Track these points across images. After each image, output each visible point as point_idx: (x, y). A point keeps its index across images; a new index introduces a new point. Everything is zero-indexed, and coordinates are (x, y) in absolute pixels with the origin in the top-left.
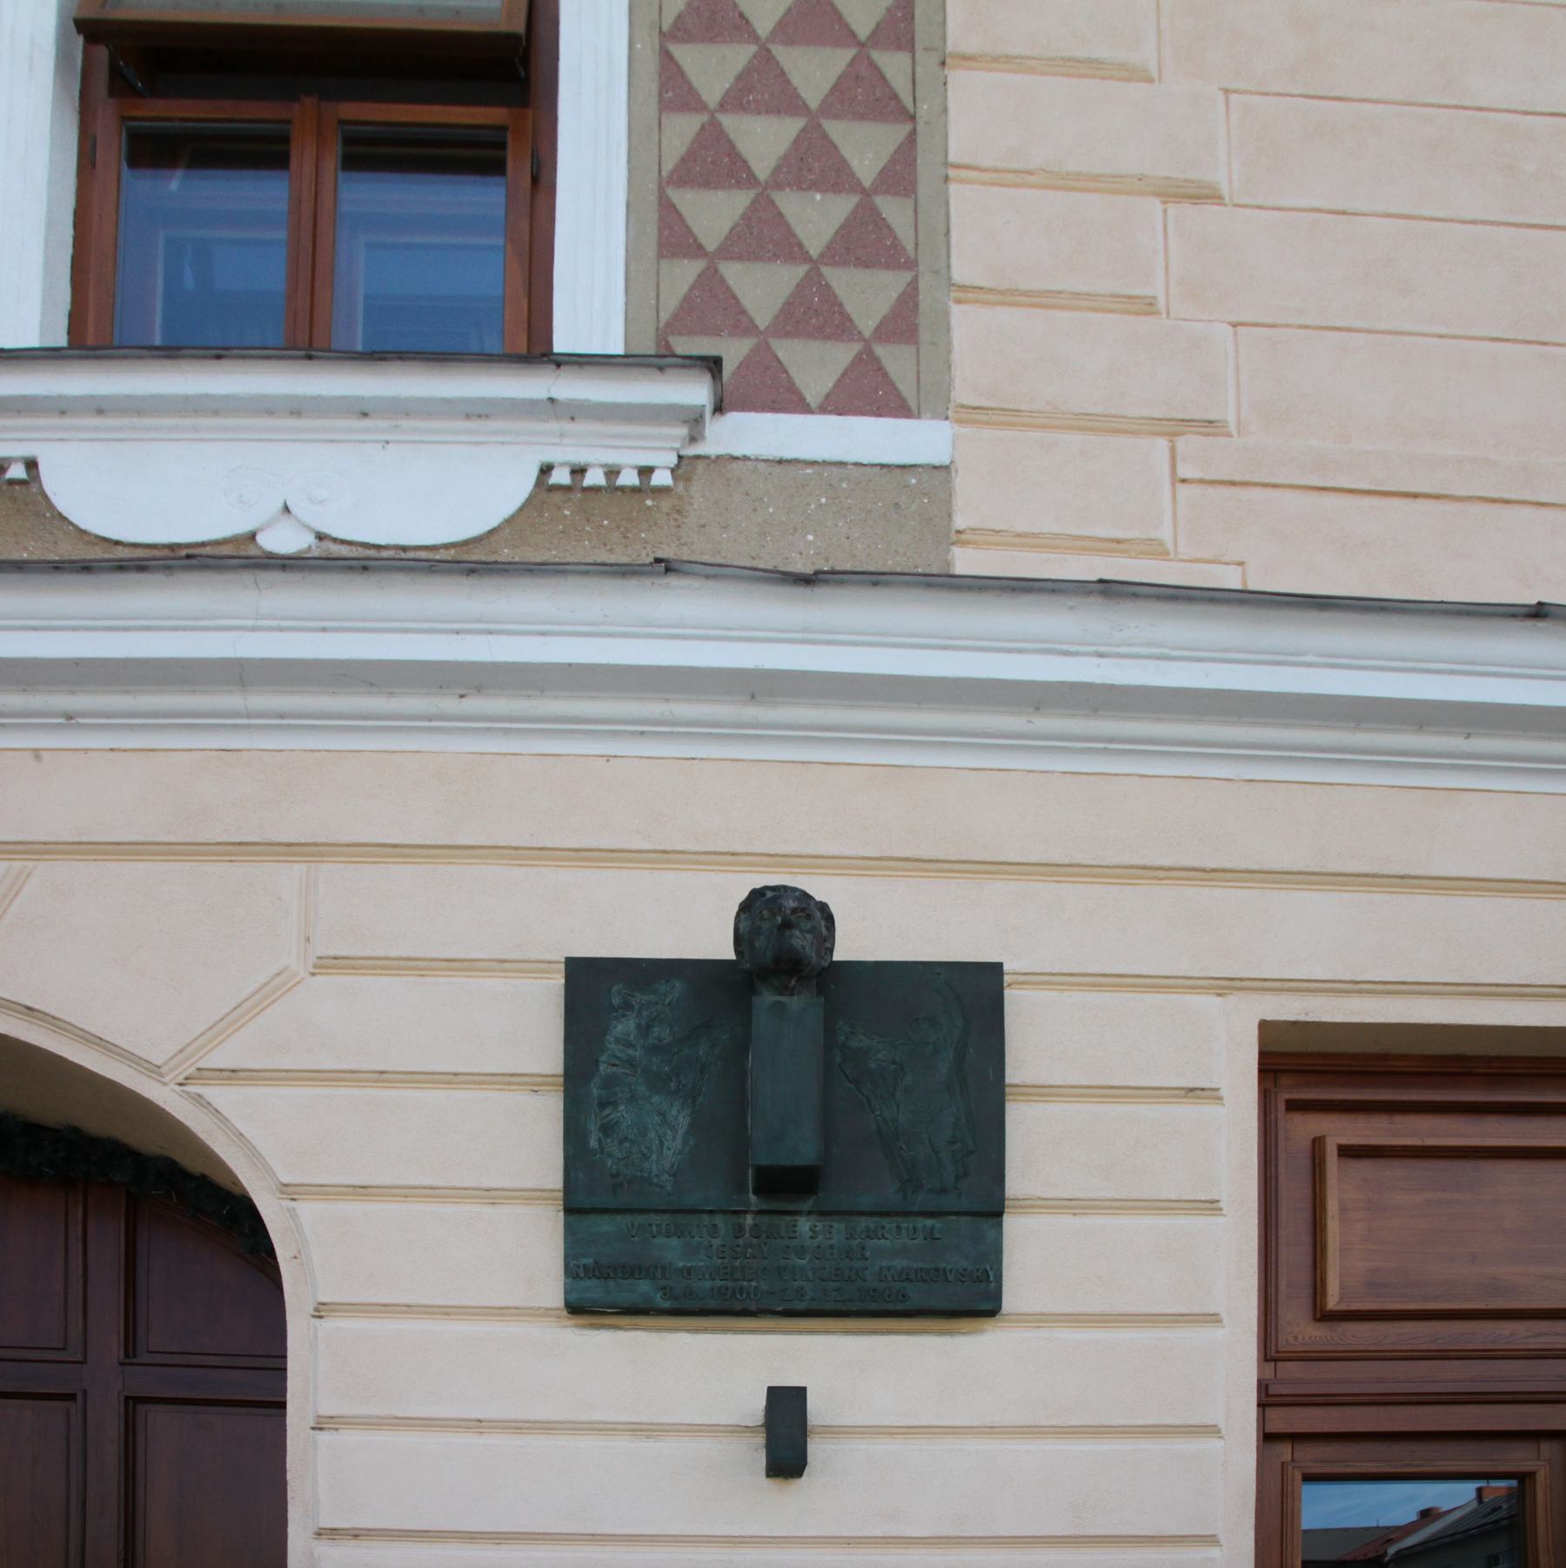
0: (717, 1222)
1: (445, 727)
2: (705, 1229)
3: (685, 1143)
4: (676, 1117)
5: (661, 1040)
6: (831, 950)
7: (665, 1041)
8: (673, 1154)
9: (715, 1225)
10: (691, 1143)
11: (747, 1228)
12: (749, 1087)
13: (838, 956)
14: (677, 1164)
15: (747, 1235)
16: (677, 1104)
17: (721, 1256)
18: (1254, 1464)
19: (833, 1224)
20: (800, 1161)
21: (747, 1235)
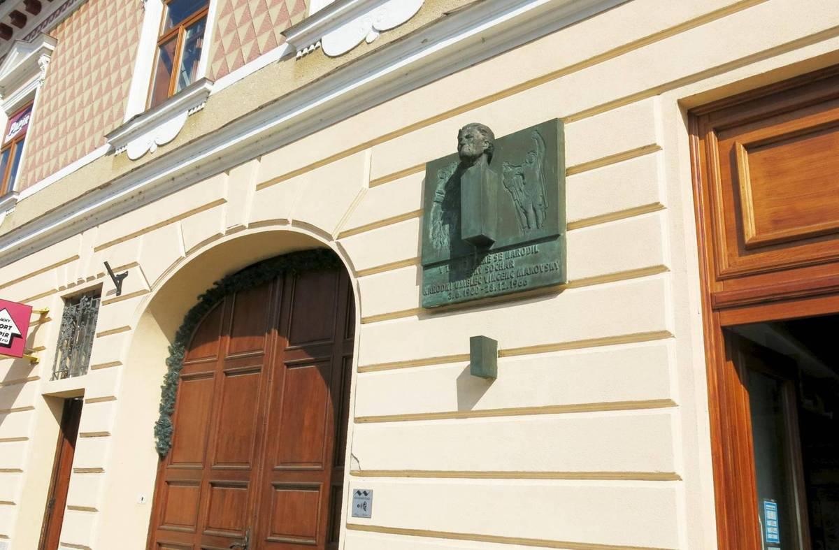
16: (454, 214)
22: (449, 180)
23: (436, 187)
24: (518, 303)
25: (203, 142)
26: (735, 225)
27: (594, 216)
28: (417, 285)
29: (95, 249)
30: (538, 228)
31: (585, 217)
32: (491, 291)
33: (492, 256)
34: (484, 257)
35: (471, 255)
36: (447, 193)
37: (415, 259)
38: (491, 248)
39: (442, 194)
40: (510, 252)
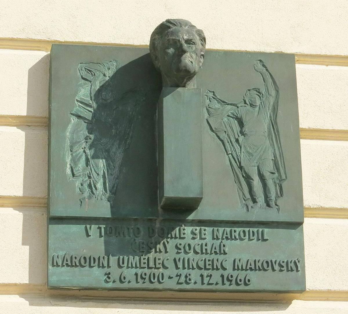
0: (139, 227)
1: (279, 143)
2: (75, 154)
3: (120, 171)
4: (115, 153)
5: (105, 100)
6: (301, 139)
7: (109, 101)
8: (114, 178)
9: (138, 228)
10: (124, 171)
11: (156, 230)
12: (157, 134)
13: (301, 140)
14: (116, 185)
15: (157, 235)
16: (116, 144)
17: (141, 250)
18: (87, 39)
19: (206, 228)
20: (191, 195)
21: (157, 235)
22: (102, 87)
23: (76, 93)
24: (245, 307)
25: (231, 129)
26: (289, 290)
27: (339, 207)
28: (23, 244)
29: (254, 203)
30: (268, 205)
31: (327, 206)
32: (187, 283)
33: (188, 230)
34: (173, 229)
35: (150, 220)
36: (98, 107)
37: (16, 198)
38: (191, 217)
39: (91, 107)
40: (221, 230)
